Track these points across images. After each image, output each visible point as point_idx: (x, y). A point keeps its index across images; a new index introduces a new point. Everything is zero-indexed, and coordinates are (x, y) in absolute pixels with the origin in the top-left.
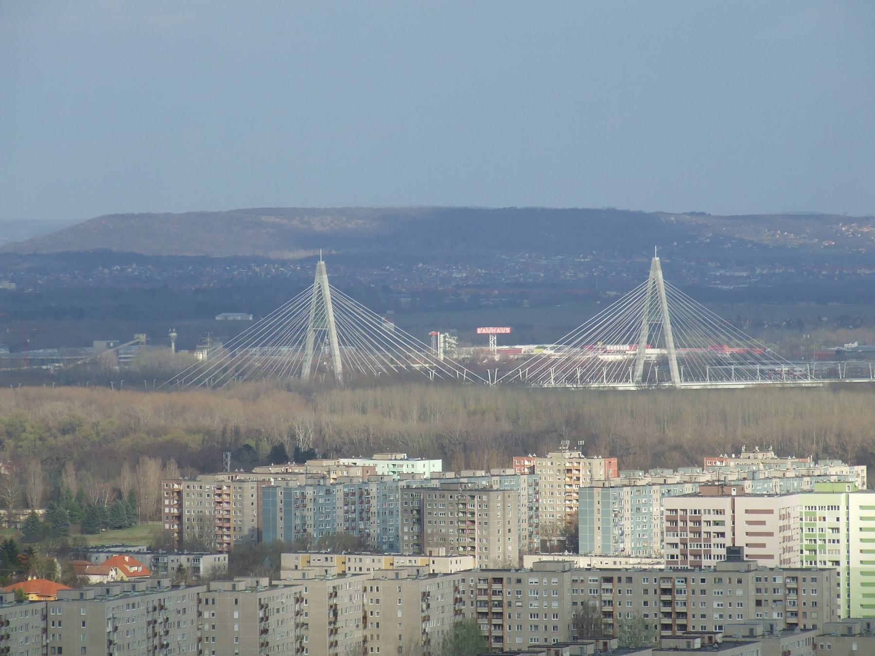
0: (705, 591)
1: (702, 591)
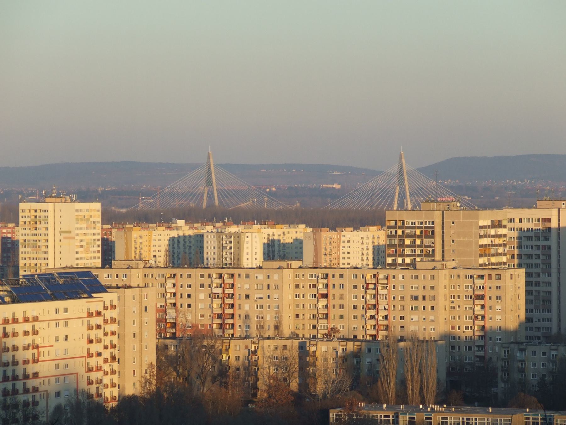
0: (343, 305)
1: (340, 305)
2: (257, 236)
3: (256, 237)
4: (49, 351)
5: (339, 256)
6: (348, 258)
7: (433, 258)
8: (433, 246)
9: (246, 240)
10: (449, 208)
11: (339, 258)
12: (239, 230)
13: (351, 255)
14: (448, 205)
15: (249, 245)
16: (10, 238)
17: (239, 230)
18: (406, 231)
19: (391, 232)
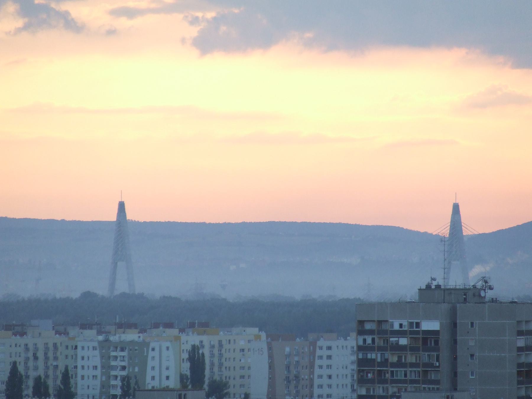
2: (170, 349)
3: (168, 348)
4: (121, 191)
5: (312, 380)
6: (330, 386)
7: (438, 386)
8: (437, 365)
9: (151, 354)
10: (465, 299)
11: (312, 386)
12: (139, 337)
13: (334, 382)
14: (465, 295)
15: (156, 363)
16: (212, 396)
17: (139, 337)
18: (391, 339)
19: (365, 340)
